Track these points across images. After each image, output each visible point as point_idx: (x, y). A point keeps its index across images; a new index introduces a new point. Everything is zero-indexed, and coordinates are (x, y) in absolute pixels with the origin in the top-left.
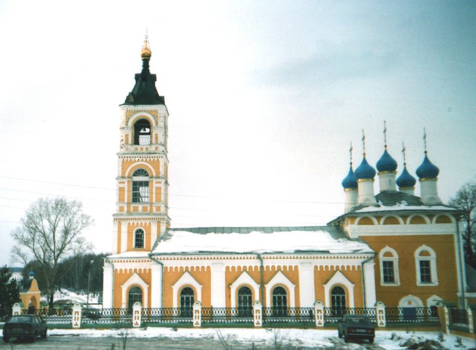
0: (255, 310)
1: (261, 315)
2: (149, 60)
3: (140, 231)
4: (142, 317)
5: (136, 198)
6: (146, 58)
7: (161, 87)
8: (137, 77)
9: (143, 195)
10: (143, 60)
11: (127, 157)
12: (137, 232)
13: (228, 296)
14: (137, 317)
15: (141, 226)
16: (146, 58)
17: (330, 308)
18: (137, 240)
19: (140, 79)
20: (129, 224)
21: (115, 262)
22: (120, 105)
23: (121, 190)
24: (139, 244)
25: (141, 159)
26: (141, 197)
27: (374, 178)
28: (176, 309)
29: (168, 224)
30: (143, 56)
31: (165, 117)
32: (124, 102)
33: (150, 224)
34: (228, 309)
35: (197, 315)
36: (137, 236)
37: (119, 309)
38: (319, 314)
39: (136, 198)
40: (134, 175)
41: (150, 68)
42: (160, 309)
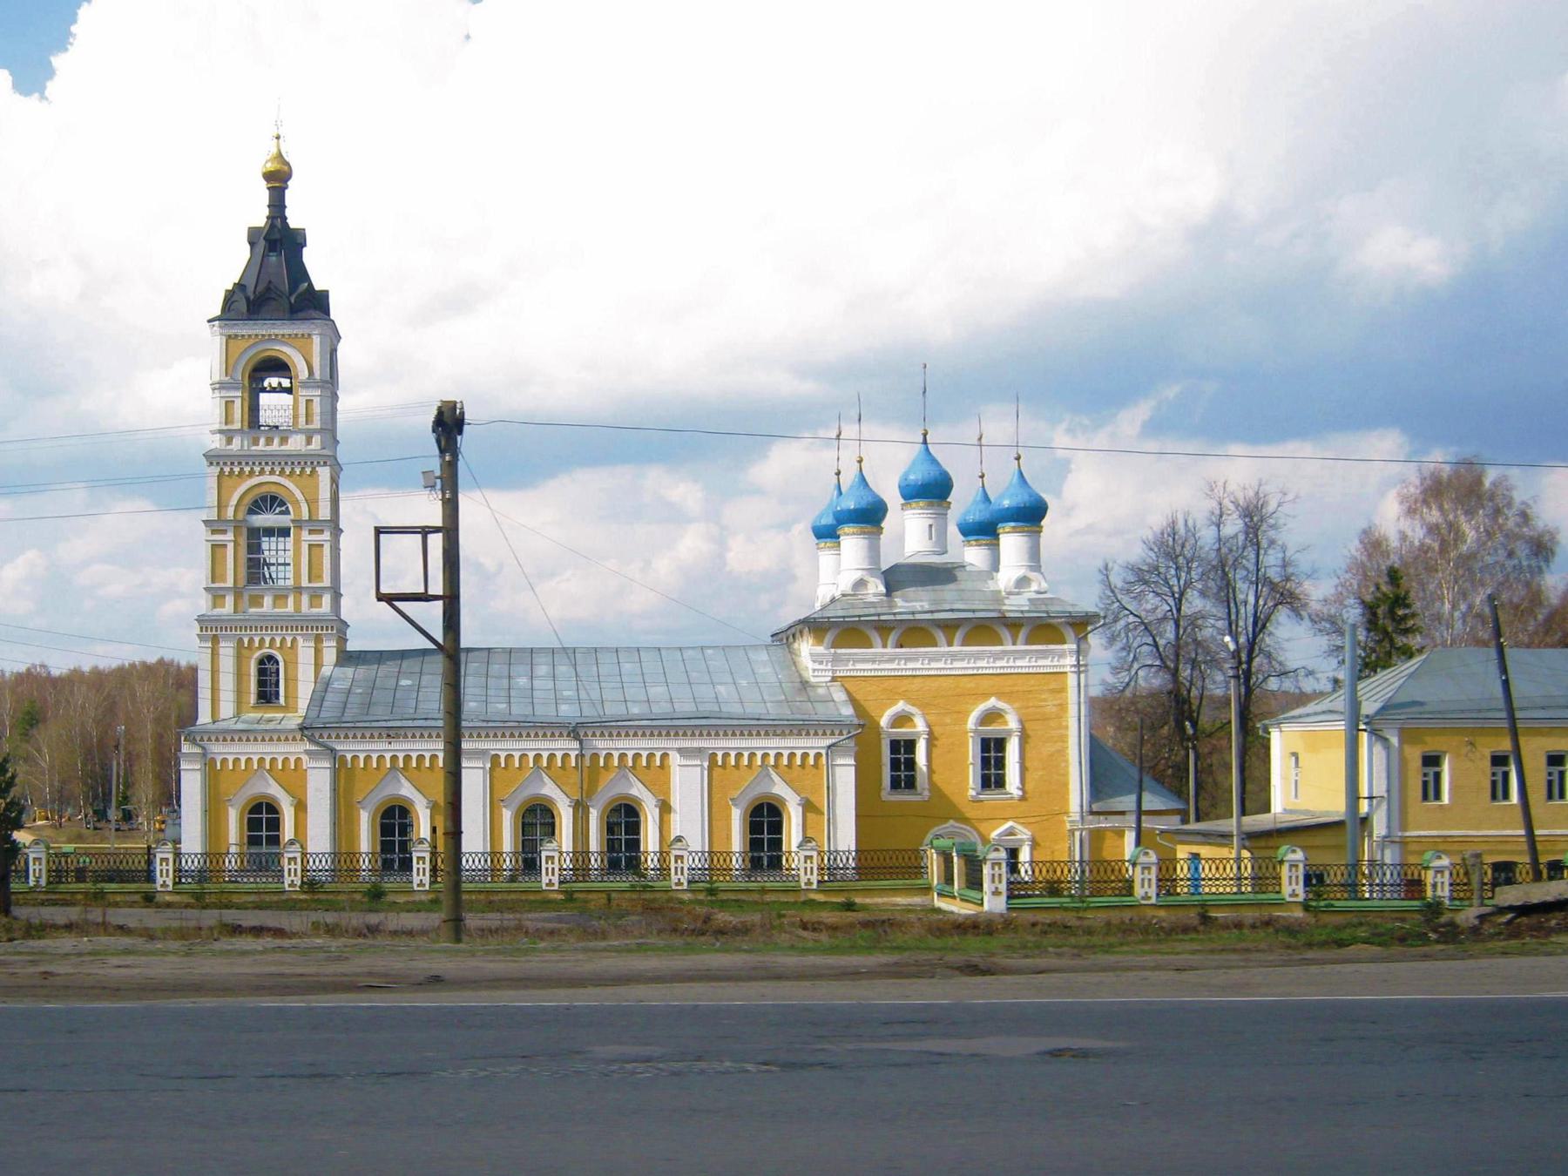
0: (544, 854)
1: (428, 866)
2: (286, 188)
3: (271, 658)
4: (303, 871)
5: (255, 570)
6: (278, 180)
7: (320, 267)
8: (254, 236)
9: (273, 561)
10: (269, 188)
11: (232, 464)
12: (261, 662)
13: (1220, 840)
14: (421, 870)
15: (270, 647)
16: (278, 180)
17: (600, 853)
18: (261, 683)
19: (262, 244)
20: (240, 641)
21: (209, 740)
22: (209, 321)
23: (217, 548)
24: (267, 694)
25: (257, 469)
26: (269, 565)
27: (882, 525)
28: (1027, 865)
29: (342, 640)
30: (269, 176)
31: (1106, 568)
32: (218, 312)
33: (294, 641)
34: (495, 854)
35: (550, 866)
36: (262, 672)
37: (353, 855)
38: (292, 866)
39: (255, 570)
40: (251, 512)
41: (288, 213)
42: (330, 854)
